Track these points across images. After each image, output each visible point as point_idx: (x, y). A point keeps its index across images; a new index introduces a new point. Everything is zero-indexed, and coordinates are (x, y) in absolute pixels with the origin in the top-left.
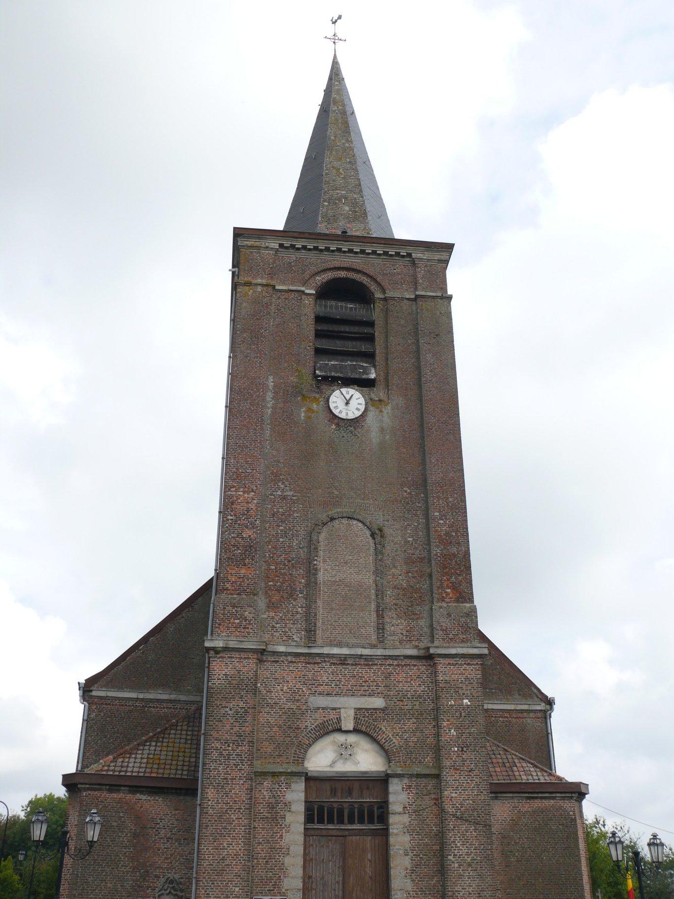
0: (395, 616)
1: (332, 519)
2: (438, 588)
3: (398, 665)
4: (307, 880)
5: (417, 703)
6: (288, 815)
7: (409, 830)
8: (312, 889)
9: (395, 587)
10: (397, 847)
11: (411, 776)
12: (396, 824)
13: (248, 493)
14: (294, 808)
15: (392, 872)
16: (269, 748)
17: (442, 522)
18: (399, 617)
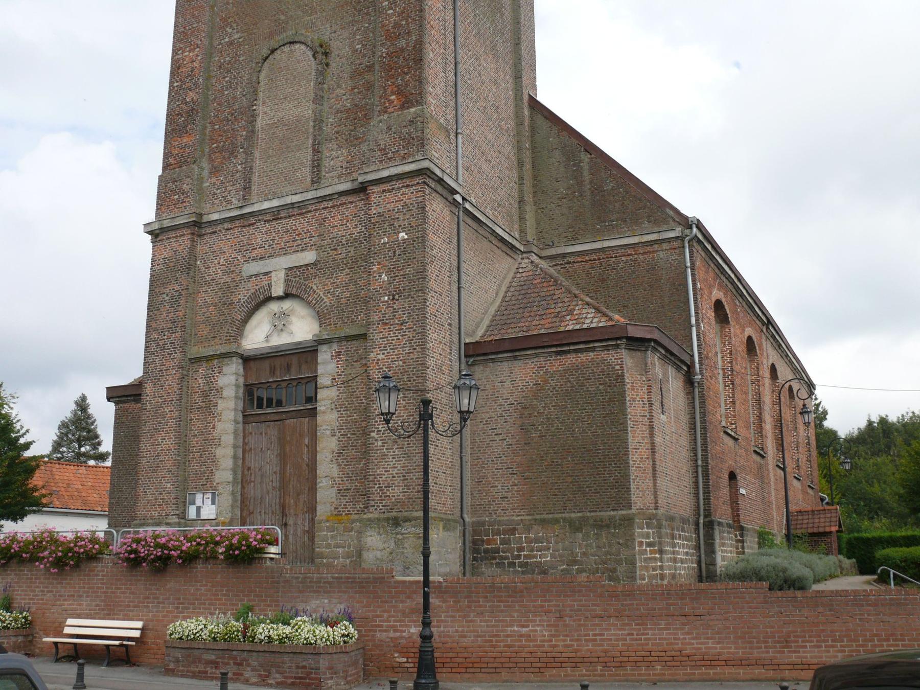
0: (335, 146)
1: (273, 51)
2: (381, 97)
3: (333, 207)
4: (246, 472)
5: (352, 249)
6: (220, 401)
7: (338, 406)
8: (251, 482)
9: (338, 111)
10: (324, 427)
11: (340, 340)
12: (324, 400)
13: (193, 50)
14: (225, 393)
15: (319, 457)
16: (205, 331)
17: (391, 11)
18: (340, 147)
